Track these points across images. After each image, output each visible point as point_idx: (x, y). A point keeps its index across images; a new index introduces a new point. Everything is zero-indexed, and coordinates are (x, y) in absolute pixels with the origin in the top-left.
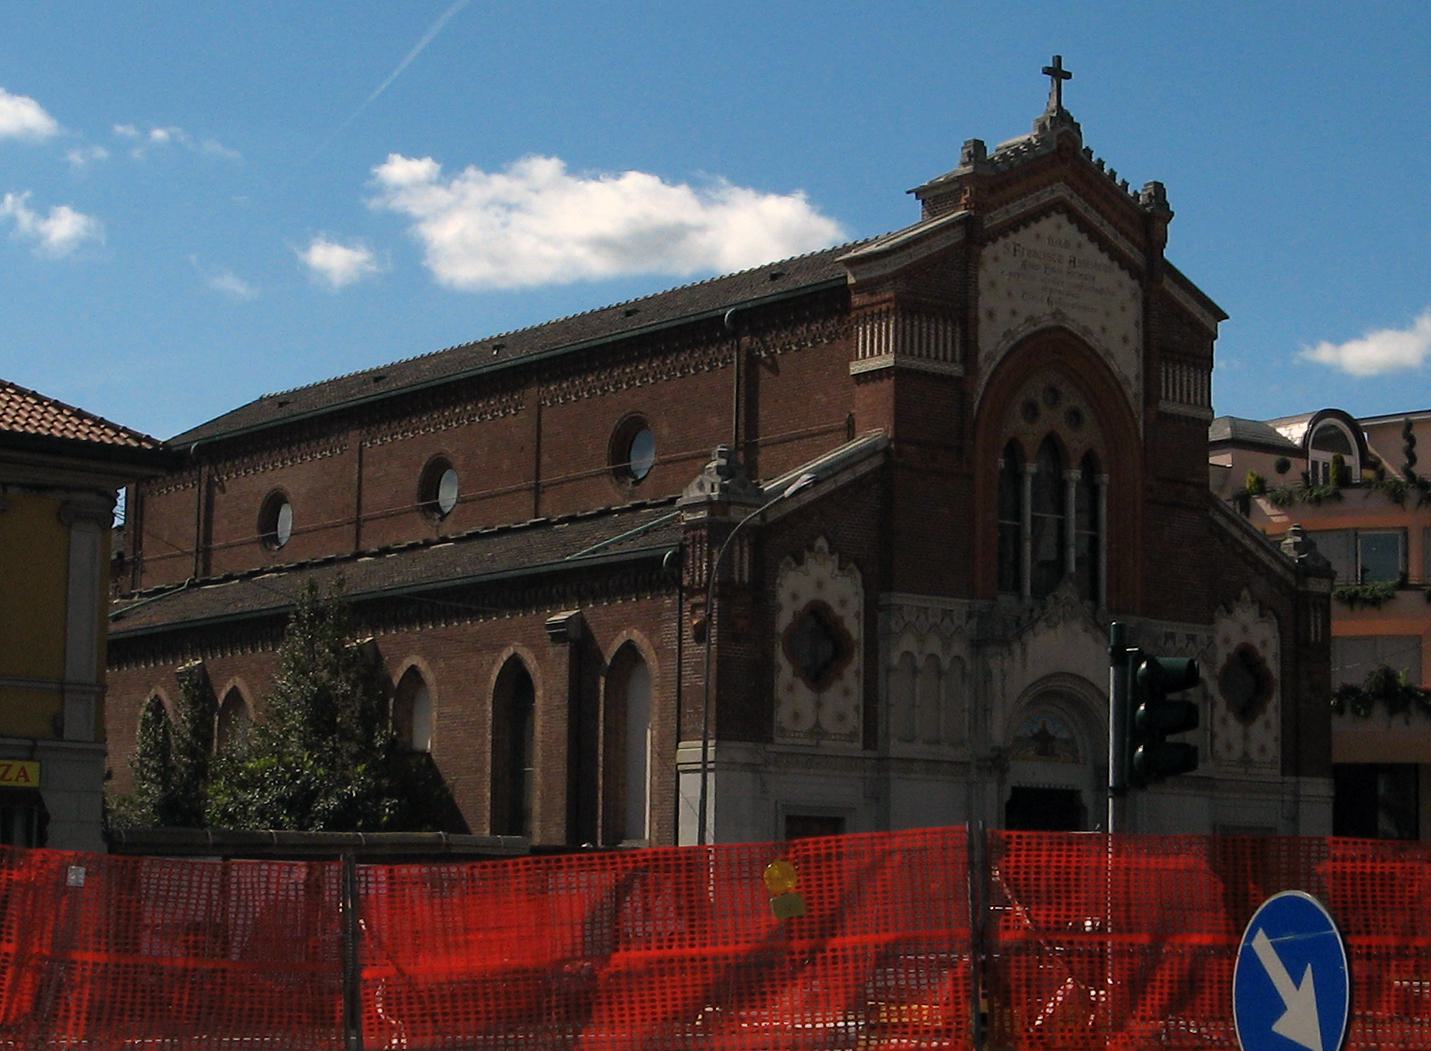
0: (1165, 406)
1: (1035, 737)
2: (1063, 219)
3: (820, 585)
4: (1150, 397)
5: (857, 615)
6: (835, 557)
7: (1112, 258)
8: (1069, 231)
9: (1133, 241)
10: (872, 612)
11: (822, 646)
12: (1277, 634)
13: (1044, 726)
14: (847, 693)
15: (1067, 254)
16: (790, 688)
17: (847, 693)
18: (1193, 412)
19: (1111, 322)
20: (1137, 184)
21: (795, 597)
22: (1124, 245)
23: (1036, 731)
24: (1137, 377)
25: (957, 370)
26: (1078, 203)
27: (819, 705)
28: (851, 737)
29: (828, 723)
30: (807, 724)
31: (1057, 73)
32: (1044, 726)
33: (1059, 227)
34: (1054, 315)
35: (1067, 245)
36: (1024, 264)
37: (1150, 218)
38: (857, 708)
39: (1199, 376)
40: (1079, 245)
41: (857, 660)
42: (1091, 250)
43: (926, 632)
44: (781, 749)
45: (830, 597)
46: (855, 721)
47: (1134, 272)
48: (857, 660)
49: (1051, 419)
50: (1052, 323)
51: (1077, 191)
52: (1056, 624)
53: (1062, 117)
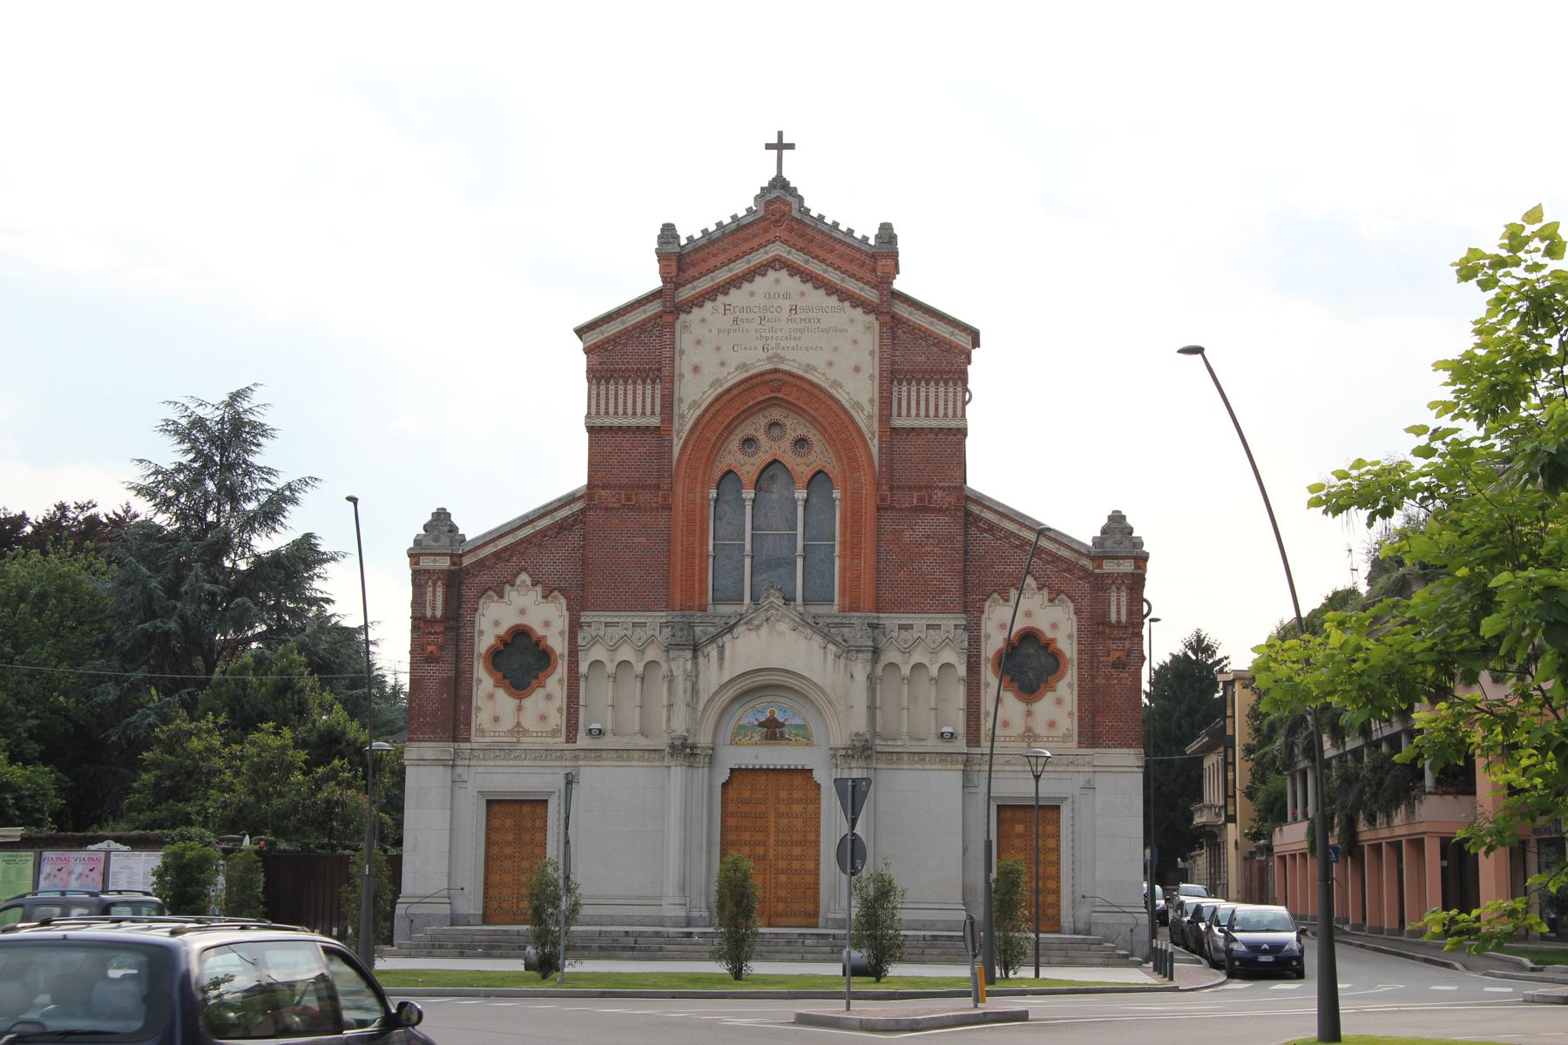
0: (898, 422)
1: (761, 725)
2: (784, 273)
3: (523, 612)
4: (885, 418)
5: (1070, 636)
6: (539, 588)
7: (841, 300)
8: (793, 284)
9: (860, 279)
10: (575, 626)
11: (521, 659)
12: (566, 614)
13: (772, 713)
14: (1059, 702)
15: (786, 304)
16: (491, 697)
17: (1059, 702)
18: (953, 424)
19: (839, 354)
20: (867, 230)
21: (497, 623)
22: (853, 286)
23: (762, 719)
24: (871, 401)
25: (655, 421)
26: (797, 258)
27: (519, 708)
28: (554, 733)
29: (1040, 728)
30: (507, 723)
31: (780, 146)
32: (772, 713)
33: (777, 281)
34: (769, 359)
35: (787, 296)
36: (736, 320)
37: (678, 257)
38: (560, 710)
39: (914, 389)
40: (802, 294)
41: (561, 670)
42: (817, 297)
43: (622, 641)
44: (475, 746)
45: (534, 622)
46: (557, 720)
47: (868, 308)
48: (561, 670)
49: (768, 449)
50: (769, 367)
51: (794, 246)
52: (758, 627)
53: (779, 183)
